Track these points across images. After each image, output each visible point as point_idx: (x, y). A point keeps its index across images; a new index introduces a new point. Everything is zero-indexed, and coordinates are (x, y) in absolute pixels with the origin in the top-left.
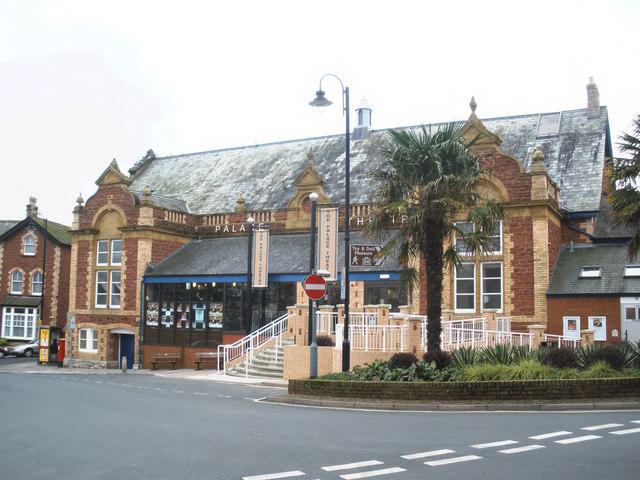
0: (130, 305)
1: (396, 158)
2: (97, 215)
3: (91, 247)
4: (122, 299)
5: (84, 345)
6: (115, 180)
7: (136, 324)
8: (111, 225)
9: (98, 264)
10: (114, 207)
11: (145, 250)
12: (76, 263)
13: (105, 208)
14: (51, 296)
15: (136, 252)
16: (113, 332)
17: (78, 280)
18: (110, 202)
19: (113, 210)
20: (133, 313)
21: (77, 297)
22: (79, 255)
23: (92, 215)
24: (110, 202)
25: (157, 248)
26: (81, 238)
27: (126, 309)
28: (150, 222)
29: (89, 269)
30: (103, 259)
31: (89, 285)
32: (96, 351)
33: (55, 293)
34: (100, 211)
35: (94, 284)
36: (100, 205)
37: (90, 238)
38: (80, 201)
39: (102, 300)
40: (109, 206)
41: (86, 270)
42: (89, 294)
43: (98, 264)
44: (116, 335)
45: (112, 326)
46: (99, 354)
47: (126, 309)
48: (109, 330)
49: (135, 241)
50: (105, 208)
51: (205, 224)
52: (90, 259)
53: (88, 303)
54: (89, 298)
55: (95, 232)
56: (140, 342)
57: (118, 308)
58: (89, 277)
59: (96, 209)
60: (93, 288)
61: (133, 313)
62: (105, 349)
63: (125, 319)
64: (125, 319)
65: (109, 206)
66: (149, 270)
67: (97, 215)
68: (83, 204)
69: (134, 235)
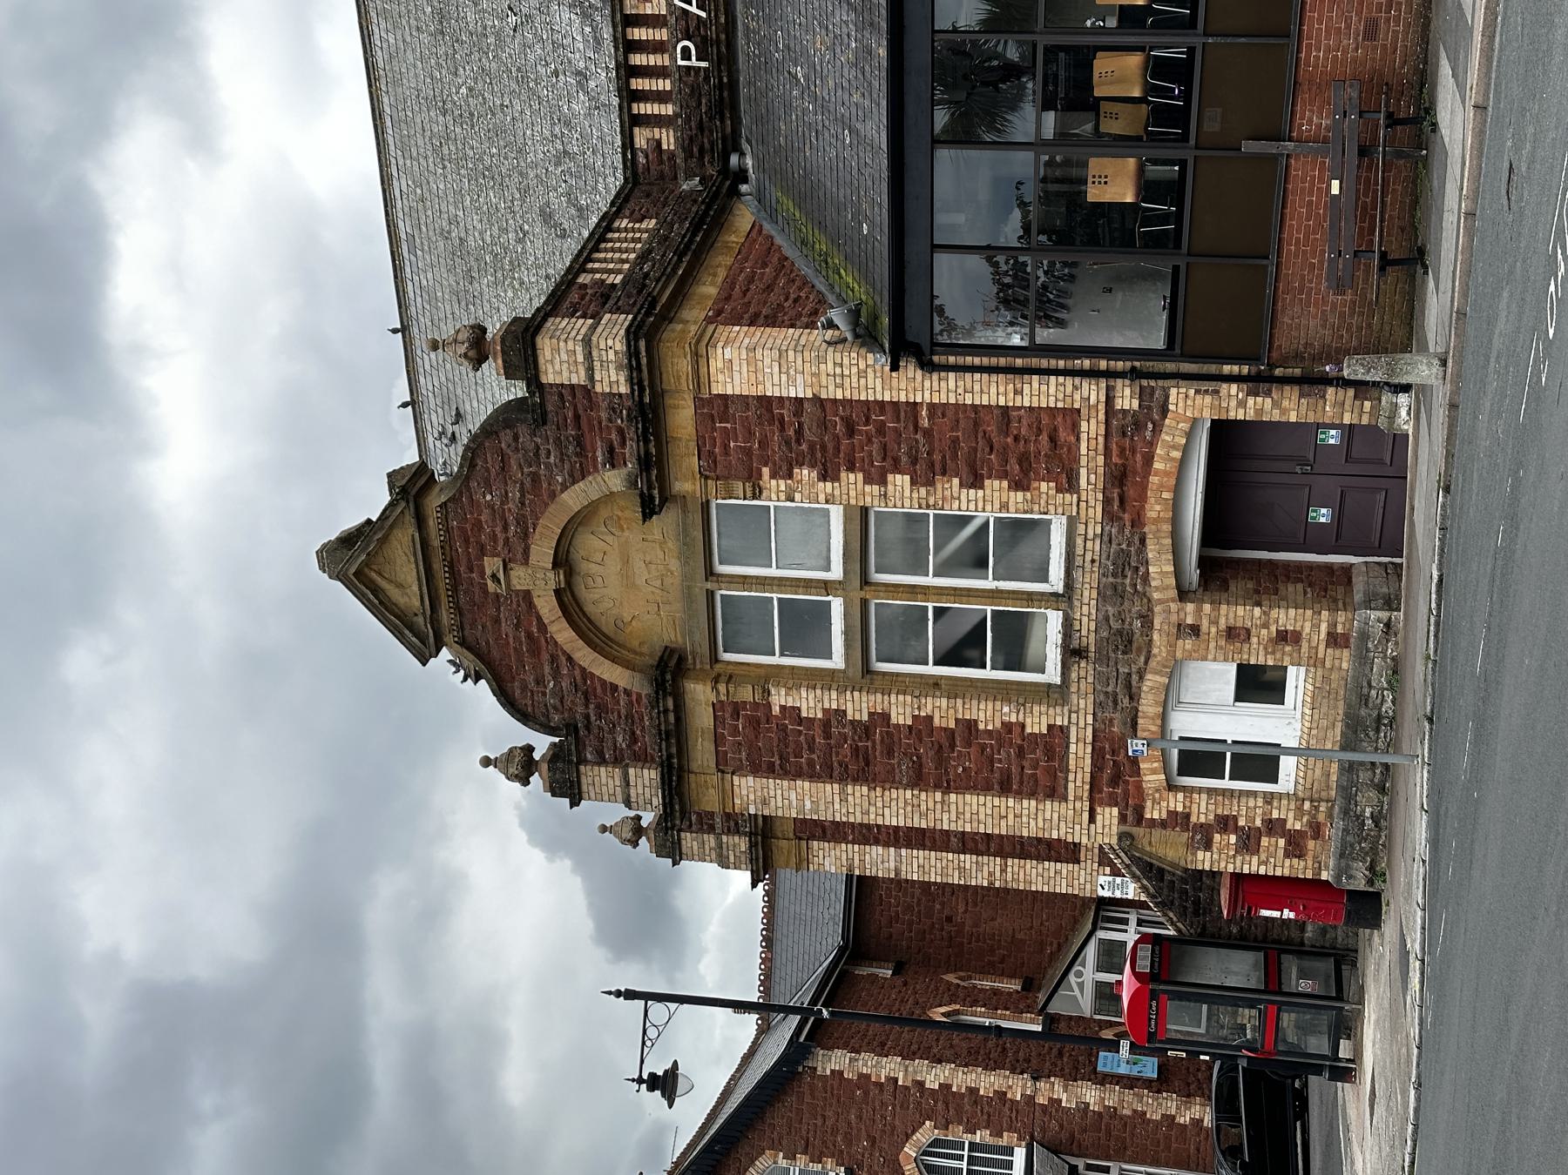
0: (1033, 450)
1: (1120, 632)
2: (585, 656)
3: (746, 694)
4: (1017, 505)
5: (1259, 762)
6: (403, 541)
7: (1153, 413)
8: (636, 578)
9: (837, 661)
10: (542, 552)
11: (753, 364)
12: (830, 789)
13: (547, 606)
14: (1030, 1100)
15: (765, 402)
16: (1193, 574)
17: (918, 780)
18: (520, 578)
19: (563, 561)
20: (1091, 429)
21: (1005, 789)
22: (787, 769)
23: (587, 686)
24: (520, 578)
25: (773, 302)
26: (702, 752)
27: (1069, 483)
28: (612, 335)
29: (858, 706)
30: (805, 626)
31: (944, 713)
32: (1297, 680)
33: (1018, 1087)
34: (563, 634)
35: (935, 684)
36: (537, 640)
37: (700, 695)
38: (520, 765)
39: (1014, 640)
40: (536, 578)
41: (864, 730)
42: (988, 715)
43: (837, 661)
44: (1206, 564)
45: (1160, 569)
46: (1314, 662)
47: (1069, 483)
48: (1183, 594)
49: (716, 408)
50: (547, 606)
51: (668, 140)
52: (810, 703)
53: (1037, 722)
54: (1009, 713)
55: (669, 670)
56: (1258, 382)
57: (1065, 522)
58: (901, 711)
59: (560, 658)
60: (956, 689)
61: (1091, 429)
62: (1286, 618)
63: (1124, 483)
64: (1124, 483)
65: (536, 578)
66: (865, 336)
67: (585, 656)
68: (542, 744)
69: (682, 419)
